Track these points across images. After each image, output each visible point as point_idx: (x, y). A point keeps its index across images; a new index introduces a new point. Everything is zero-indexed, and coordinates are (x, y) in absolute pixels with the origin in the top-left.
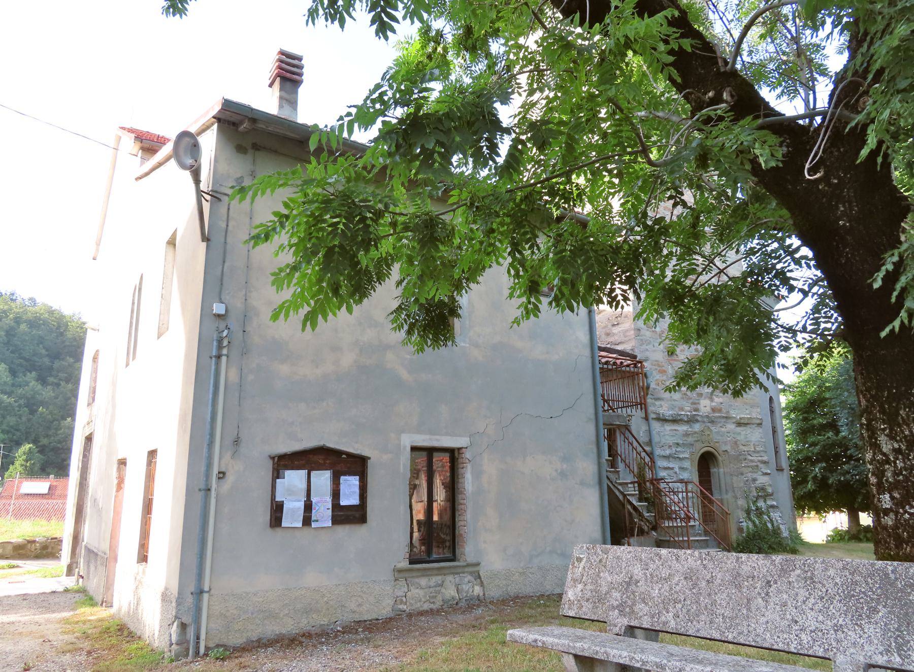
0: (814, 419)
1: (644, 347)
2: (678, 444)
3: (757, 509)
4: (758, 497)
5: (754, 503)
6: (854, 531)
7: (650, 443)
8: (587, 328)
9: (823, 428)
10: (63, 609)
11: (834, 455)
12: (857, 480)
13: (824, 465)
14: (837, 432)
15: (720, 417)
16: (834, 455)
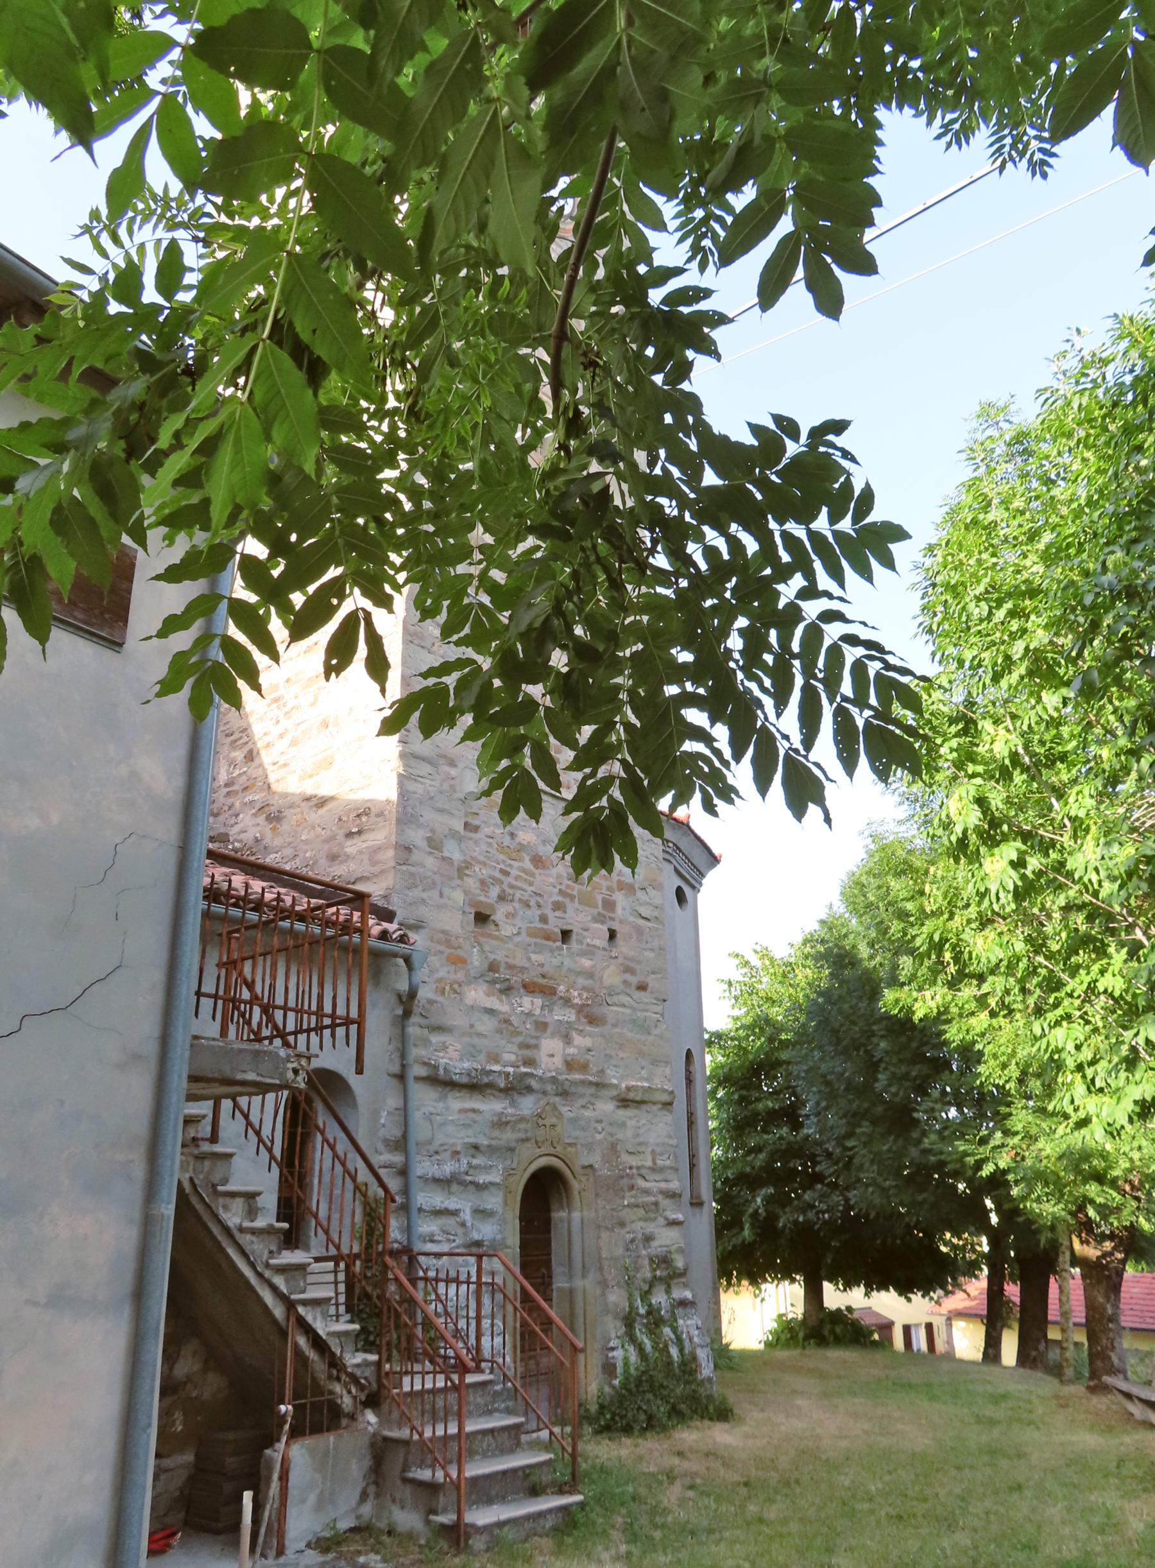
0: (758, 1100)
1: (416, 893)
2: (476, 1147)
3: (649, 1313)
4: (652, 1283)
5: (646, 1295)
6: (813, 1321)
7: (401, 1144)
8: (181, 751)
9: (773, 1117)
10: (228, 1256)
11: (789, 1171)
12: (825, 1222)
13: (771, 1190)
14: (797, 1126)
15: (583, 1082)
16: (789, 1171)
